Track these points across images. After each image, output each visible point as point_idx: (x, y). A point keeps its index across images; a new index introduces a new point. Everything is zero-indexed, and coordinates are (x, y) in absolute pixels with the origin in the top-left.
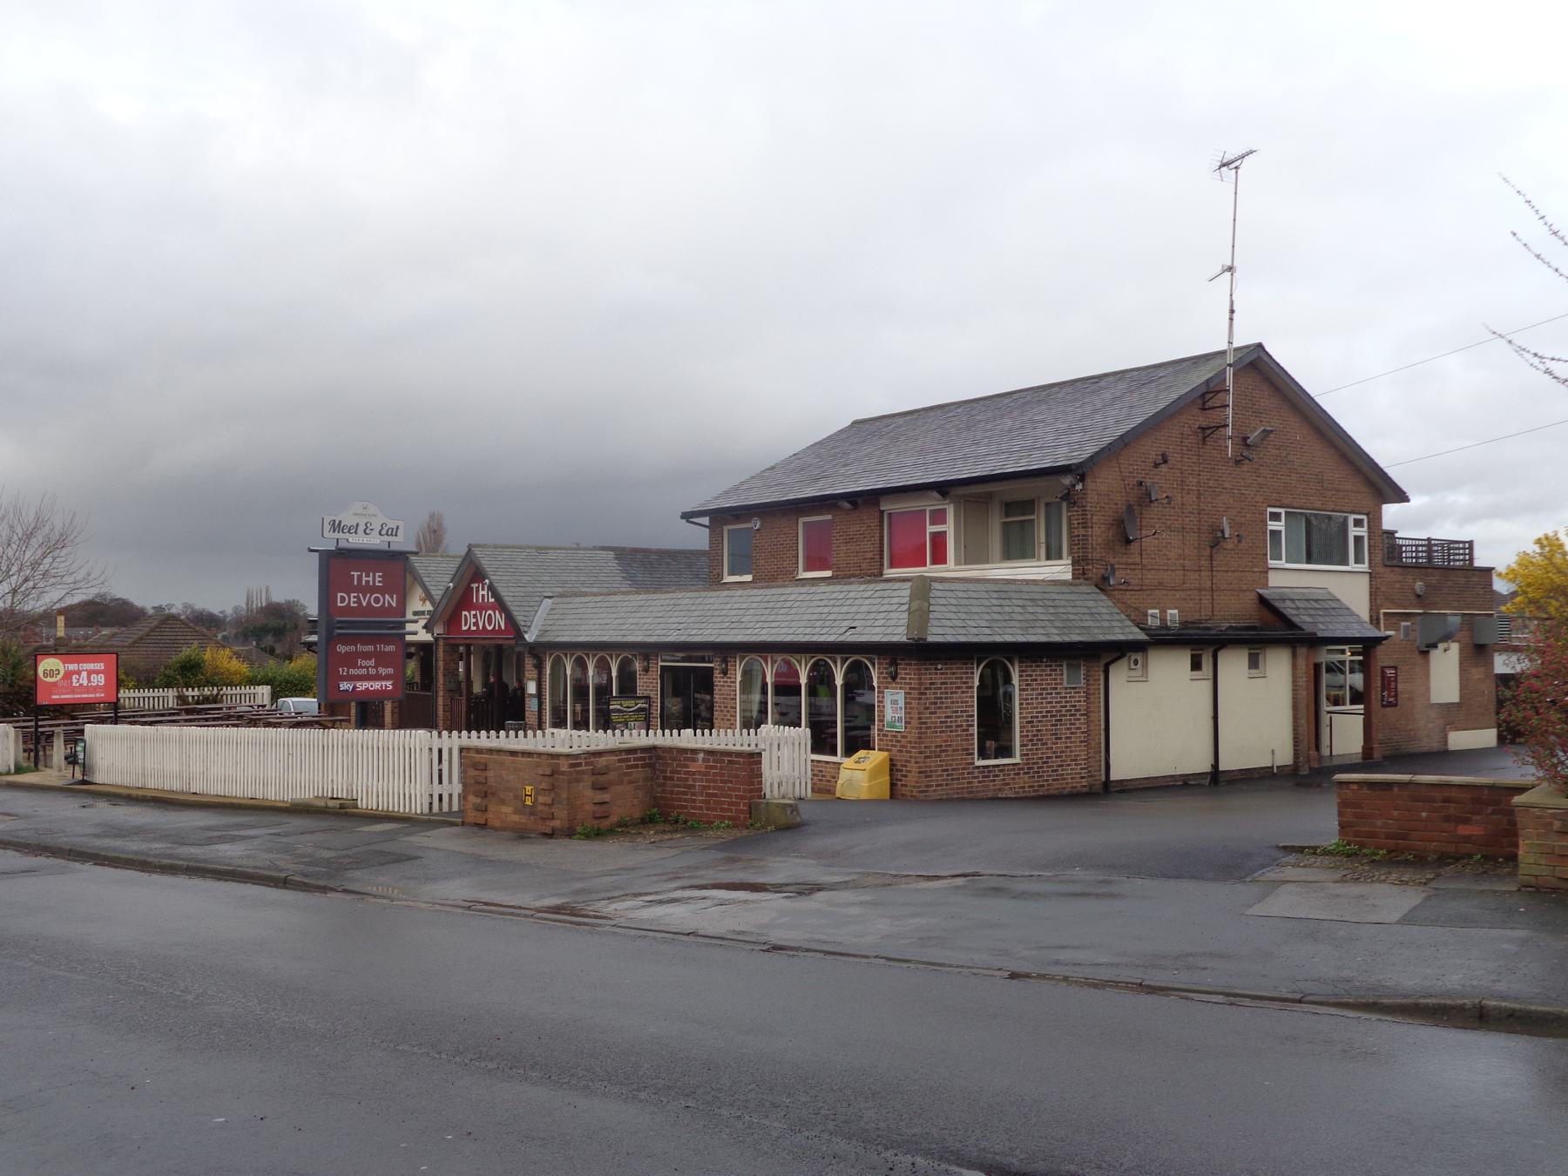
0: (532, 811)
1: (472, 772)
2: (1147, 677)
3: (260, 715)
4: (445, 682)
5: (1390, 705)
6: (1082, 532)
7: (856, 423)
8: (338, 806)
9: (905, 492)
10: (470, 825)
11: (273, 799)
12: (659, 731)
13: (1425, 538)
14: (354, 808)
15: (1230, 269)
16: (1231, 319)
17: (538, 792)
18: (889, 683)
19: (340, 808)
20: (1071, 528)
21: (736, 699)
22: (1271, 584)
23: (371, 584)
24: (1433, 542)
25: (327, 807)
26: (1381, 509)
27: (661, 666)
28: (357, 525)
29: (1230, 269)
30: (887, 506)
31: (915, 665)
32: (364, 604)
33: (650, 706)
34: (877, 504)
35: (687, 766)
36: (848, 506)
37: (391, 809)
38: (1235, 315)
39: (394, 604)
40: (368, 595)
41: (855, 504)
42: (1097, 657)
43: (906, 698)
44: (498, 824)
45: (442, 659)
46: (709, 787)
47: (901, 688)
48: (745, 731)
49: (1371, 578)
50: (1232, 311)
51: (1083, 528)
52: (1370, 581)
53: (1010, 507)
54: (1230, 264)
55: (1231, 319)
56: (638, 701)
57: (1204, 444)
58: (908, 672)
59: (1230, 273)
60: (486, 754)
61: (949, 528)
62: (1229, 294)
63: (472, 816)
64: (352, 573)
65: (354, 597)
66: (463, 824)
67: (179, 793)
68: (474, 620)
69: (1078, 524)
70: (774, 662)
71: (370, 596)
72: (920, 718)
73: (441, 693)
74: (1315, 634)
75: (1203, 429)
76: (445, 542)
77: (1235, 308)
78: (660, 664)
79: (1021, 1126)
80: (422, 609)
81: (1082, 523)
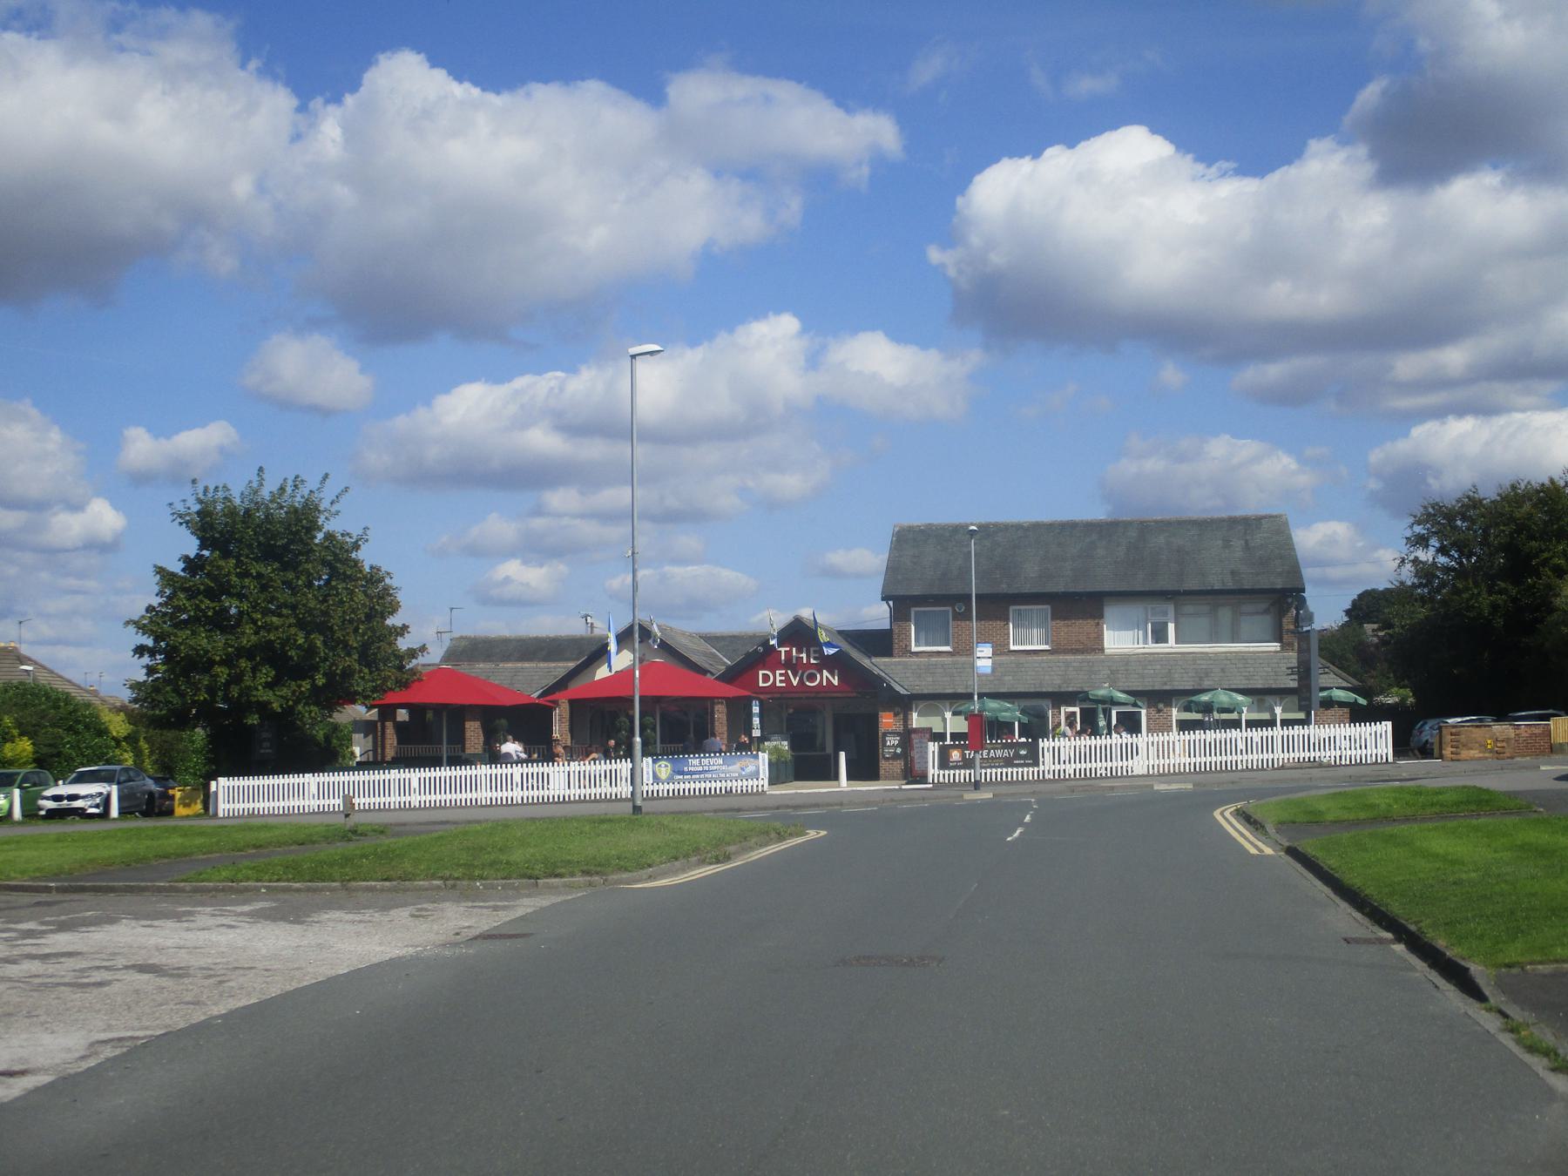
20: (383, 761)
23: (805, 662)
32: (795, 683)
39: (836, 682)
40: (800, 672)
65: (781, 675)
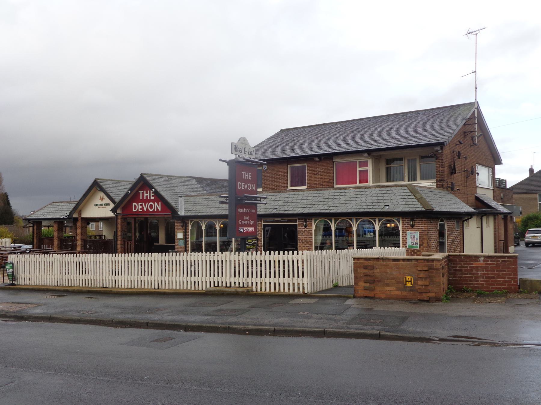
0: (411, 289)
1: (362, 271)
2: (469, 226)
3: (17, 250)
4: (121, 234)
5: (411, 237)
6: (441, 169)
7: (282, 131)
8: (246, 291)
9: (416, 147)
10: (360, 297)
11: (45, 285)
12: (263, 253)
13: (498, 178)
14: (252, 292)
15: (475, 72)
16: (476, 91)
17: (416, 280)
18: (409, 228)
19: (247, 292)
21: (312, 238)
22: (477, 193)
24: (500, 180)
25: (236, 291)
26: (495, 166)
27: (263, 224)
28: (242, 148)
29: (475, 72)
30: (336, 160)
31: (425, 220)
33: (257, 242)
34: (332, 159)
35: (472, 264)
36: (317, 159)
37: (90, 286)
38: (477, 89)
41: (320, 159)
42: (461, 218)
43: (419, 235)
44: (383, 296)
45: (120, 224)
46: (488, 274)
47: (416, 231)
48: (237, 253)
49: (493, 191)
50: (476, 88)
51: (442, 168)
52: (493, 193)
53: (389, 161)
54: (475, 70)
55: (476, 91)
56: (253, 240)
57: (465, 138)
58: (422, 224)
59: (475, 74)
60: (373, 261)
61: (370, 168)
62: (475, 82)
63: (361, 293)
64: (243, 172)
66: (354, 297)
67: (38, 286)
68: (141, 207)
69: (439, 166)
70: (379, 221)
71: (248, 184)
72: (428, 243)
73: (120, 239)
74: (500, 211)
75: (465, 132)
76: (3, 184)
77: (477, 87)
78: (263, 223)
79: (202, 373)
80: (101, 203)
81: (441, 166)
